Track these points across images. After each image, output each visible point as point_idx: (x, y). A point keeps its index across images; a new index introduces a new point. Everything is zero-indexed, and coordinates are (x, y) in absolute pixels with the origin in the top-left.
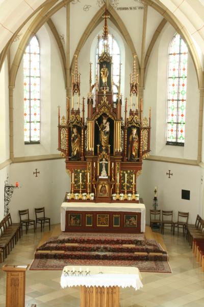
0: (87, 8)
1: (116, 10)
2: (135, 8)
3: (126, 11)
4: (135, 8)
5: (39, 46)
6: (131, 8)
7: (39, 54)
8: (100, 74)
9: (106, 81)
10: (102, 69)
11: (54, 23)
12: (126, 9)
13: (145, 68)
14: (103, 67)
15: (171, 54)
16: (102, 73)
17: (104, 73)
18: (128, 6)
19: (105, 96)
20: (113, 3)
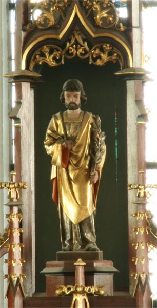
8: (43, 162)
9: (90, 209)
10: (56, 123)
14: (61, 107)
16: (55, 151)
17: (66, 154)
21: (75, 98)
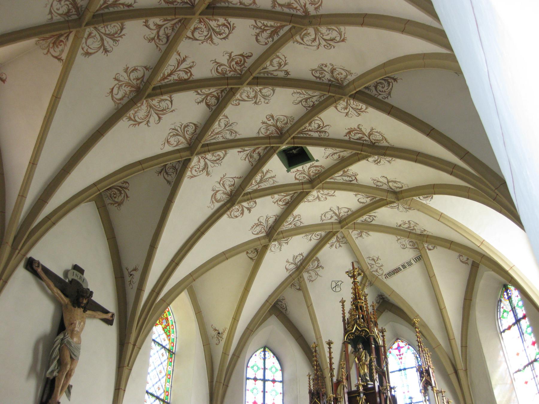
0: (336, 286)
1: (385, 280)
2: (410, 264)
3: (399, 275)
4: (410, 264)
5: (282, 370)
6: (404, 267)
7: (282, 382)
11: (300, 330)
12: (396, 271)
13: (466, 370)
15: (504, 331)
18: (398, 264)
19: (362, 395)
20: (375, 268)
21: (361, 346)
